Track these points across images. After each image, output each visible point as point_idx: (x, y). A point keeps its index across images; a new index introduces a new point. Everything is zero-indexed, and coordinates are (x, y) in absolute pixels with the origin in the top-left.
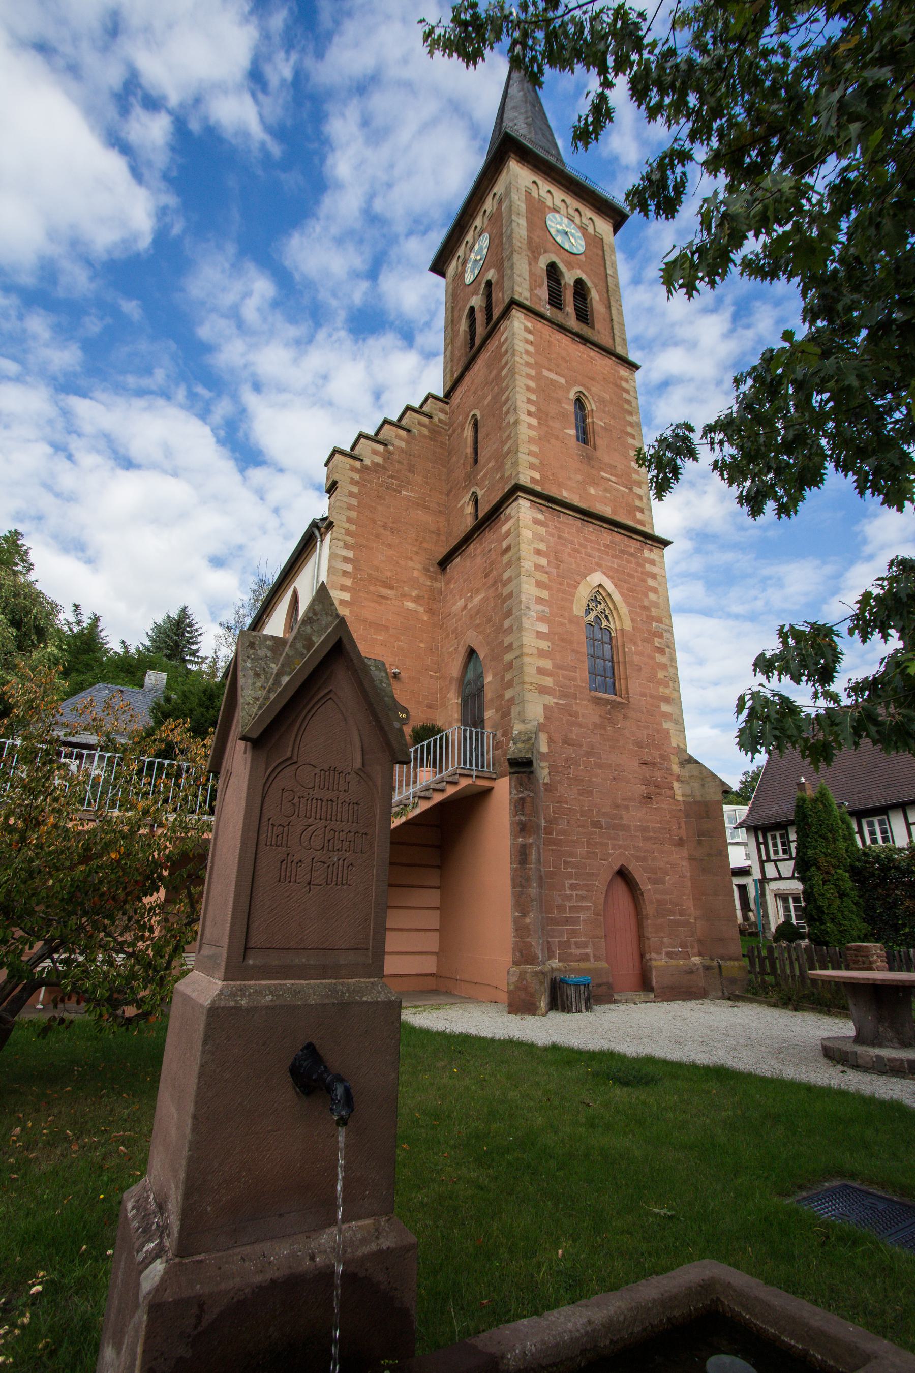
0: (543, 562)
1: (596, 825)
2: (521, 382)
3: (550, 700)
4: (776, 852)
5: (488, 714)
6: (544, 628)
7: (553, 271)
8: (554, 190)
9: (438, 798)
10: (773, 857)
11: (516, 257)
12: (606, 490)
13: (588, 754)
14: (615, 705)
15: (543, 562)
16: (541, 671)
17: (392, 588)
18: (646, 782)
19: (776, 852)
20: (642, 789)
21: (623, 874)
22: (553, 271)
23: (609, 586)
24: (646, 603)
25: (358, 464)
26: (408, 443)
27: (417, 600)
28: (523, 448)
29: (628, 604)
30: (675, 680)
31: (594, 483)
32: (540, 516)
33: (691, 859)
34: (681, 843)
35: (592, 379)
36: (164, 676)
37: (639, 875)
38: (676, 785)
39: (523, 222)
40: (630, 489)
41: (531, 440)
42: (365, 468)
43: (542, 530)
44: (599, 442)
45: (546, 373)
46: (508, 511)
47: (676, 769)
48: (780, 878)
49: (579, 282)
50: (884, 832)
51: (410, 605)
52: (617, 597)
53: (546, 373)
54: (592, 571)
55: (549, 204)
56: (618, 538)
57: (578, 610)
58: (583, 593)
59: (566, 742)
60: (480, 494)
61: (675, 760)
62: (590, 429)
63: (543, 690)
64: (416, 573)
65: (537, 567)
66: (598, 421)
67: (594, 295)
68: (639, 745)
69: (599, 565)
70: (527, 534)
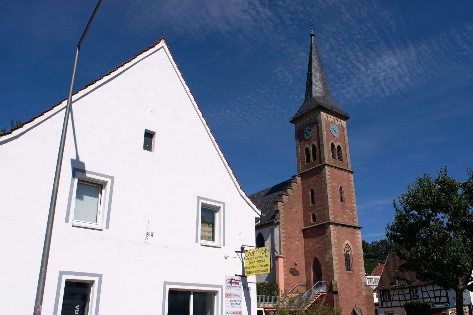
1: (348, 302)
3: (339, 275)
4: (386, 299)
8: (331, 116)
10: (385, 300)
13: (346, 287)
14: (351, 274)
17: (293, 239)
18: (358, 292)
19: (386, 299)
20: (357, 293)
23: (349, 244)
26: (293, 193)
27: (298, 241)
31: (345, 214)
33: (367, 308)
34: (364, 305)
35: (343, 181)
38: (364, 291)
41: (337, 264)
42: (285, 204)
43: (335, 232)
44: (345, 201)
47: (363, 288)
48: (387, 307)
49: (339, 146)
50: (416, 293)
51: (297, 243)
52: (351, 246)
54: (345, 240)
55: (330, 121)
58: (344, 246)
59: (342, 284)
60: (316, 215)
61: (363, 285)
62: (343, 197)
63: (337, 273)
64: (298, 233)
65: (335, 242)
66: (345, 194)
67: (342, 149)
68: (356, 283)
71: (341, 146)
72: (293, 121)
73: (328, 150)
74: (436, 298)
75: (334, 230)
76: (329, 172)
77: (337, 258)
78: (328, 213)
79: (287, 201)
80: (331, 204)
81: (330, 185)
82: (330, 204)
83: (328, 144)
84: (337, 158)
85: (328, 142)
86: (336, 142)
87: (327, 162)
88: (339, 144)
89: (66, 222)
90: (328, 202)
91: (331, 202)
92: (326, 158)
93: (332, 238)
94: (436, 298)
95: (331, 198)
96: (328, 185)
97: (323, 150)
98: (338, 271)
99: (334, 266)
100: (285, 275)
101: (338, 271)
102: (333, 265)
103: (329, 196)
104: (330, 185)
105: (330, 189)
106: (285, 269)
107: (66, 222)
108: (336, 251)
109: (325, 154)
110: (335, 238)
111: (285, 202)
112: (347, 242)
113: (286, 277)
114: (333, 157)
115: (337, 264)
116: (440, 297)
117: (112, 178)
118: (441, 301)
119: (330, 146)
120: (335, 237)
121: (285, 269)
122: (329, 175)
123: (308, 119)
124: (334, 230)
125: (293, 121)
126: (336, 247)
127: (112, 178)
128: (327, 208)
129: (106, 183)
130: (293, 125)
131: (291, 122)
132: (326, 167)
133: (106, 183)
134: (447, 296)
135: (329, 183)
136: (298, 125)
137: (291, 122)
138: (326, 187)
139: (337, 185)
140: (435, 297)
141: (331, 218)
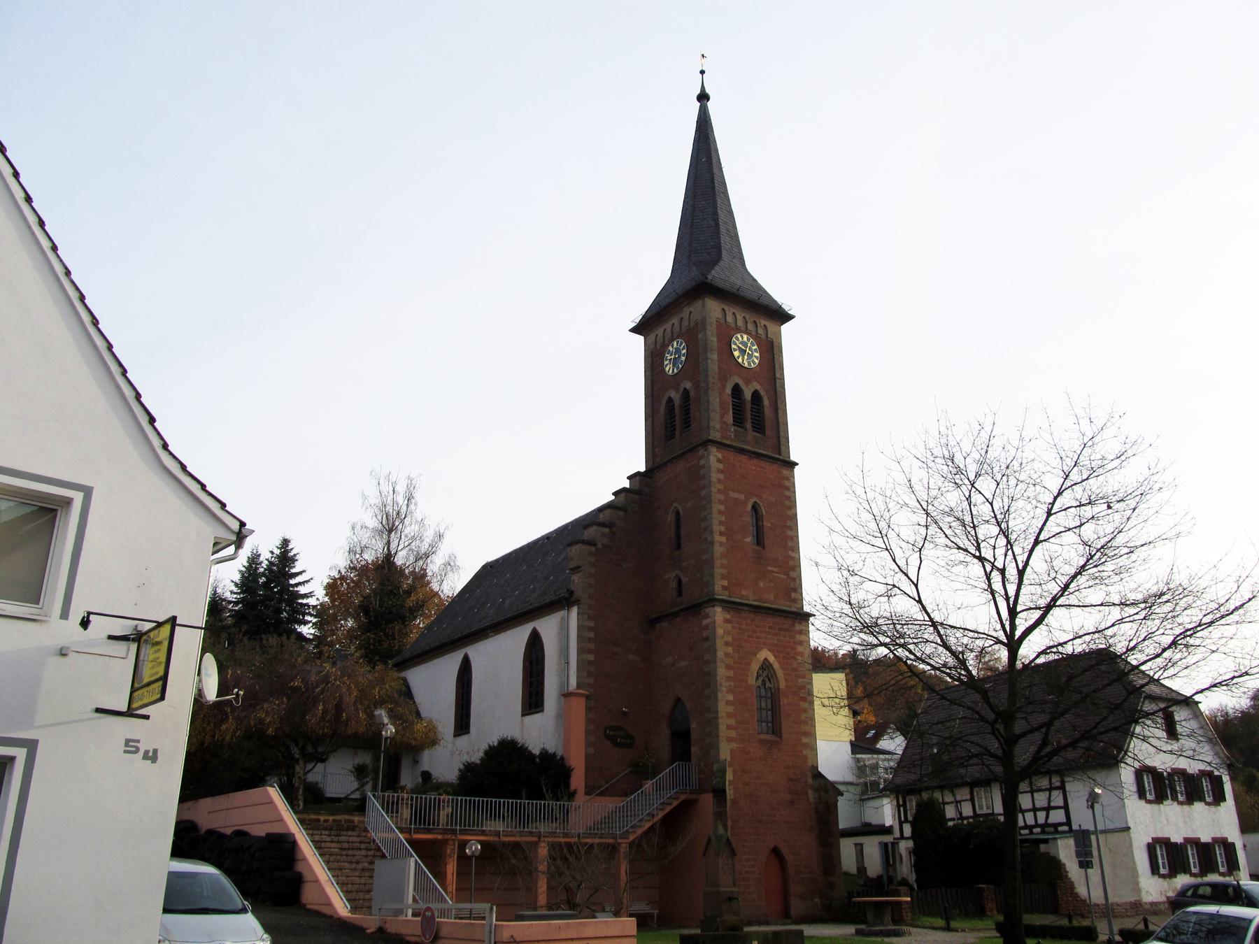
0: (730, 650)
2: (717, 507)
3: (734, 745)
5: (694, 749)
6: (730, 698)
7: (737, 390)
9: (669, 809)
11: (710, 392)
12: (771, 581)
15: (730, 650)
16: (729, 727)
21: (776, 852)
22: (737, 390)
23: (772, 659)
24: (795, 665)
25: (593, 549)
28: (717, 563)
29: (783, 669)
30: (813, 719)
32: (728, 616)
36: (377, 712)
37: (785, 851)
38: (810, 792)
39: (715, 356)
40: (788, 575)
41: (729, 715)
43: (729, 626)
45: (732, 494)
46: (707, 610)
47: (810, 781)
51: (631, 657)
52: (776, 666)
53: (732, 494)
56: (778, 620)
57: (752, 680)
58: (755, 667)
60: (684, 580)
61: (809, 774)
63: (730, 740)
65: (727, 655)
67: (766, 402)
69: (764, 644)
70: (720, 631)
71: (763, 393)
72: (640, 328)
73: (722, 403)
74: (1039, 813)
75: (726, 621)
76: (719, 461)
77: (730, 698)
78: (712, 575)
79: (606, 541)
80: (723, 549)
81: (722, 497)
82: (718, 550)
83: (724, 386)
84: (749, 426)
85: (723, 380)
86: (748, 382)
87: (715, 435)
88: (758, 387)
89: (61, 618)
90: (712, 543)
91: (721, 544)
92: (716, 424)
93: (719, 643)
94: (1039, 813)
95: (721, 534)
96: (717, 497)
97: (708, 401)
98: (733, 734)
99: (720, 721)
100: (588, 744)
101: (733, 734)
102: (717, 718)
103: (717, 528)
104: (722, 497)
105: (722, 508)
106: (592, 727)
107: (61, 618)
108: (728, 678)
109: (712, 414)
110: (727, 644)
111: (599, 546)
112: (765, 654)
113: (591, 750)
114: (739, 420)
115: (729, 715)
116: (1048, 809)
117: (88, 492)
118: (1050, 821)
119: (729, 391)
120: (729, 639)
121: (592, 727)
122: (719, 471)
123: (675, 320)
124: (726, 621)
125: (640, 328)
126: (728, 667)
127: (88, 492)
128: (710, 563)
129: (68, 502)
130: (642, 338)
131: (634, 330)
132: (713, 449)
133: (68, 502)
134: (1066, 807)
135: (719, 491)
136: (652, 337)
137: (634, 330)
138: (710, 502)
139: (742, 497)
140: (1035, 810)
141: (718, 588)
